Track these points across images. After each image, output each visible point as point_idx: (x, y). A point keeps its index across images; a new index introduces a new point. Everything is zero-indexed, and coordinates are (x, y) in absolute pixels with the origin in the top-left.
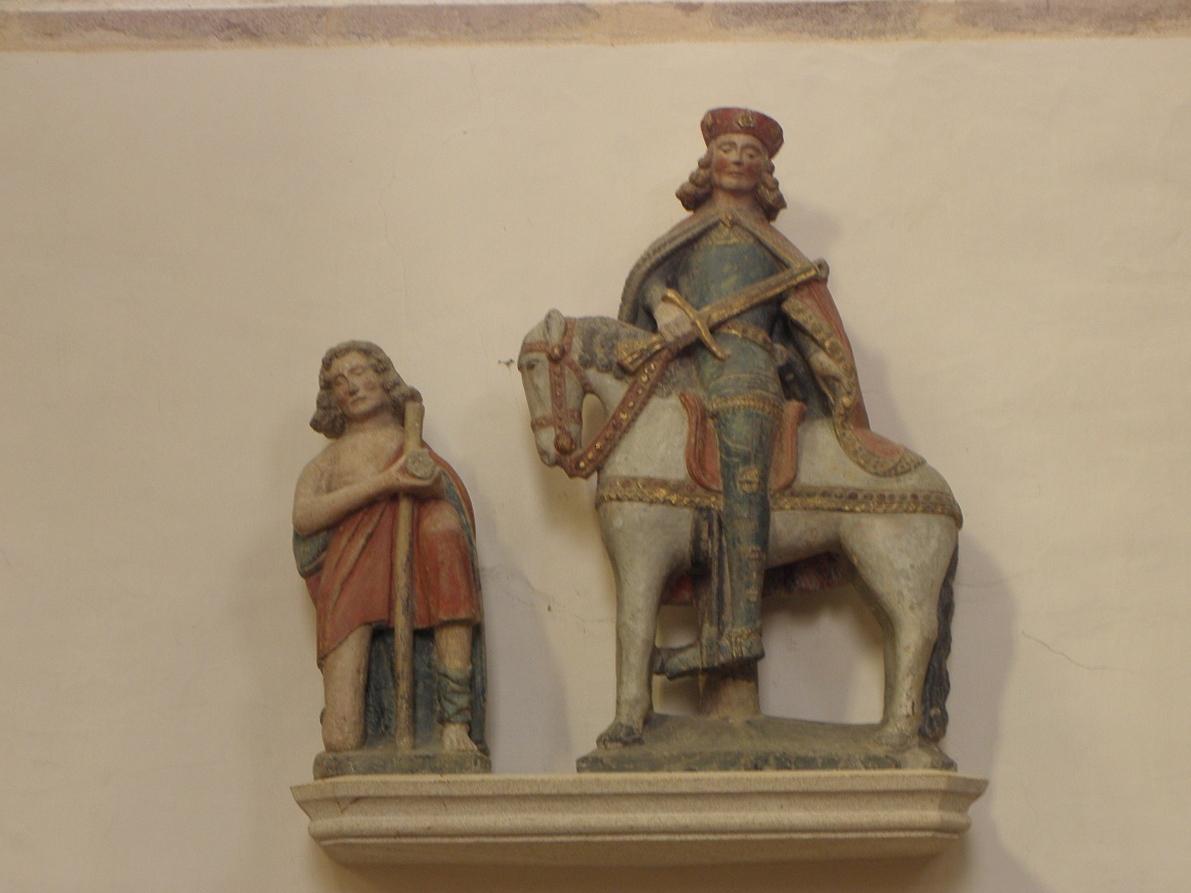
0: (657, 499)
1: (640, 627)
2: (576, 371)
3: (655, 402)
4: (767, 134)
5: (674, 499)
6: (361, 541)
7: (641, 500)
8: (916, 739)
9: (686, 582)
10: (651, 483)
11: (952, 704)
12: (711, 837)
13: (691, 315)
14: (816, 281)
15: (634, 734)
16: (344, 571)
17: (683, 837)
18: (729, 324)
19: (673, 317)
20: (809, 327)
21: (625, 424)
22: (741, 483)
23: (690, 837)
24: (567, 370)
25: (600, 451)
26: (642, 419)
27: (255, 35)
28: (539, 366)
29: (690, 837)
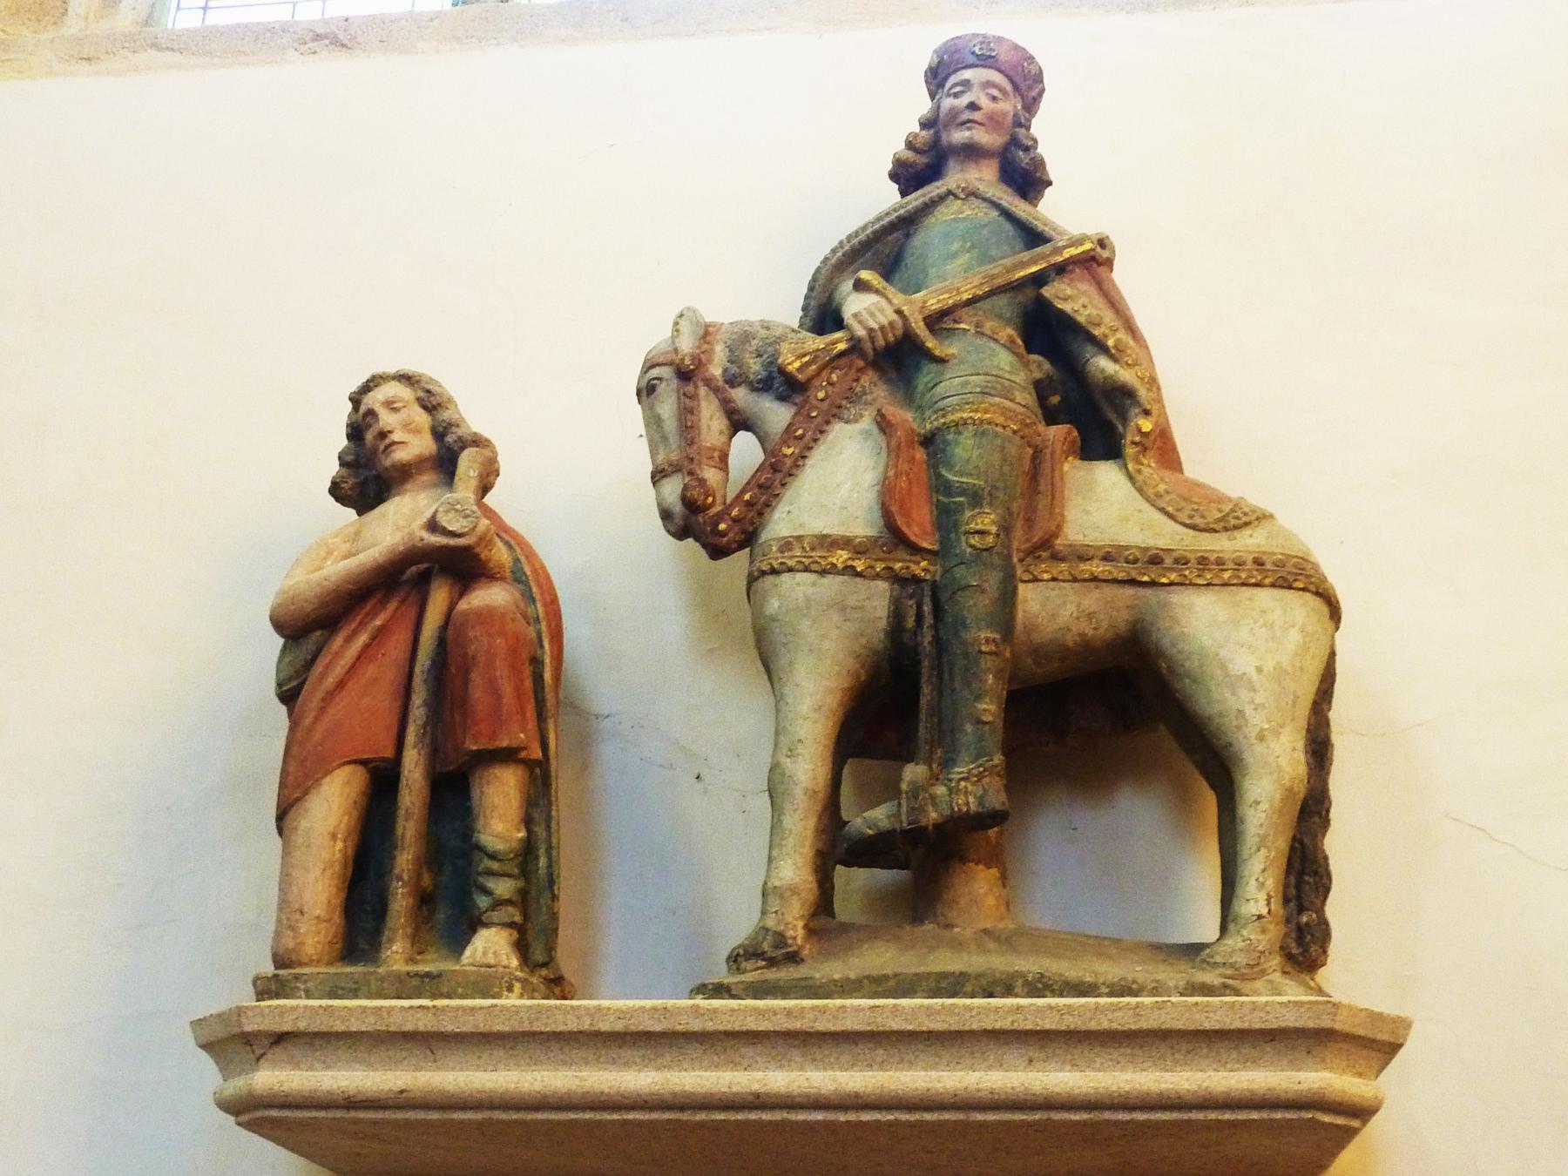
0: (834, 565)
1: (808, 767)
2: (716, 390)
3: (838, 429)
4: (1026, 83)
5: (860, 565)
6: (363, 638)
7: (807, 569)
8: (1276, 961)
9: (884, 713)
10: (830, 543)
11: (1336, 909)
12: (904, 1117)
13: (895, 301)
14: (1094, 262)
15: (786, 945)
16: (331, 680)
17: (852, 1116)
18: (956, 315)
19: (868, 309)
20: (1081, 319)
21: (789, 462)
22: (967, 533)
23: (866, 1117)
24: (703, 390)
25: (749, 504)
26: (816, 456)
27: (343, 45)
28: (662, 387)
29: (866, 1117)
